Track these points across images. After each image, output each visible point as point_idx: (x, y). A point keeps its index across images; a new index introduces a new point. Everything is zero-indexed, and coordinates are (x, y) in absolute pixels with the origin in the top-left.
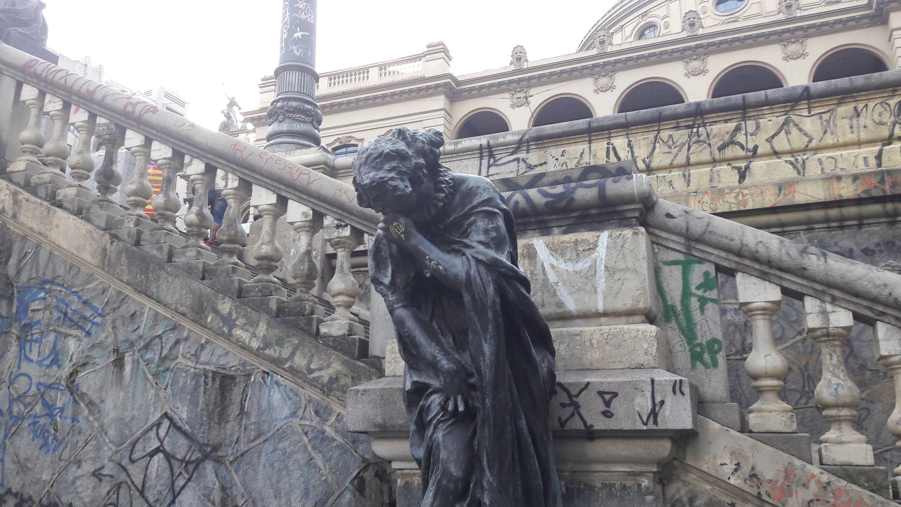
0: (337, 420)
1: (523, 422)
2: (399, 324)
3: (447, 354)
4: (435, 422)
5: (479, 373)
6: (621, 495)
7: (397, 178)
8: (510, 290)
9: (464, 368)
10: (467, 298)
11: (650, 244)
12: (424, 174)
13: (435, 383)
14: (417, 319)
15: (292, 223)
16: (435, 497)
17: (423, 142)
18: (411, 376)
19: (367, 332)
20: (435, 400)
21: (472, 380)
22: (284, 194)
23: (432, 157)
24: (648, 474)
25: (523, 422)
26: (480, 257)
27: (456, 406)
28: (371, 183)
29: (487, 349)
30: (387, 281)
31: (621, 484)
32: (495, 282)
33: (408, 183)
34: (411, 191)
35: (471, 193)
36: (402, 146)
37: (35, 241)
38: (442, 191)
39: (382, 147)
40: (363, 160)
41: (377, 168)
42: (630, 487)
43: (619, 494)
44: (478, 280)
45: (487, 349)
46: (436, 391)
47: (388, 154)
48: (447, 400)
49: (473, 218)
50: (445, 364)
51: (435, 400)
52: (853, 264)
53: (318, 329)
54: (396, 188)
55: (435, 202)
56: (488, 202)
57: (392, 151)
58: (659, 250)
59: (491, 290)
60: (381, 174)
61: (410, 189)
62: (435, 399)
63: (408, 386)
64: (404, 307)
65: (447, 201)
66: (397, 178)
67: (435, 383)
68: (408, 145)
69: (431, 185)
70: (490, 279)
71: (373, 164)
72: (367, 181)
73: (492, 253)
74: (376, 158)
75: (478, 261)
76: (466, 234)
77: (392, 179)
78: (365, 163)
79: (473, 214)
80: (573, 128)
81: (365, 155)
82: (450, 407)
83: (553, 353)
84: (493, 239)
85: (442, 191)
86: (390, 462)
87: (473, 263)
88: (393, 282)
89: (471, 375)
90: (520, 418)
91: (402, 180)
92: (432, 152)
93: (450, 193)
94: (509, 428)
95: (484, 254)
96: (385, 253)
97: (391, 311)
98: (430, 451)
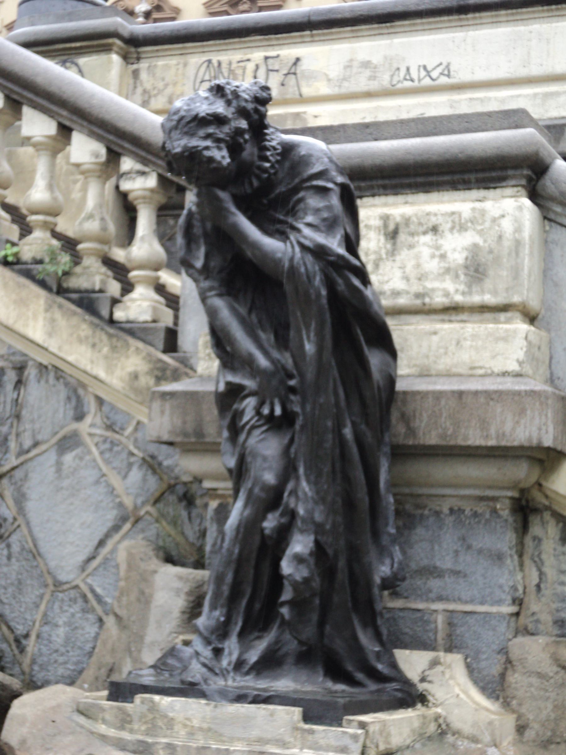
0: (136, 430)
1: (348, 432)
2: (212, 314)
3: (266, 353)
4: (248, 427)
5: (302, 375)
6: (469, 523)
7: (213, 147)
8: (340, 281)
9: (284, 368)
10: (288, 288)
11: (542, 218)
12: (246, 141)
13: (250, 383)
14: (233, 310)
15: (78, 165)
16: (246, 506)
17: (246, 101)
18: (224, 377)
19: (176, 317)
20: (250, 403)
21: (292, 383)
22: (67, 123)
23: (256, 117)
24: (504, 500)
25: (348, 432)
26: (307, 243)
27: (272, 410)
28: (183, 152)
29: (309, 348)
30: (199, 264)
31: (471, 510)
32: (322, 270)
33: (225, 153)
34: (229, 164)
35: (305, 161)
36: (220, 108)
37: (510, 494)
38: (267, 160)
39: (196, 107)
40: (174, 123)
41: (191, 134)
42: (481, 514)
43: (467, 522)
44: (303, 270)
45: (309, 348)
46: (252, 394)
47: (203, 118)
48: (261, 404)
49: (301, 194)
50: (263, 362)
51: (250, 403)
52: (209, 350)
53: (111, 314)
54: (211, 160)
55: (257, 171)
56: (321, 175)
57: (208, 114)
58: (551, 227)
59: (318, 281)
60: (195, 142)
61: (228, 160)
62: (249, 403)
63: (222, 387)
64: (220, 295)
65: (272, 171)
66: (213, 147)
67: (250, 383)
68: (229, 103)
69: (256, 151)
70: (317, 268)
71: (186, 129)
72: (178, 150)
73: (320, 239)
74: (189, 122)
75: (303, 247)
76: (293, 212)
77: (207, 148)
78: (176, 128)
79: (302, 189)
80: (494, 13)
81: (176, 117)
82: (266, 411)
83: (393, 353)
84: (324, 220)
85: (267, 160)
86: (200, 481)
87: (297, 249)
88: (206, 266)
89: (290, 376)
90: (345, 426)
91: (219, 149)
92: (256, 111)
93: (277, 162)
94: (330, 436)
95: (311, 240)
96: (197, 230)
97: (204, 299)
98: (242, 461)
